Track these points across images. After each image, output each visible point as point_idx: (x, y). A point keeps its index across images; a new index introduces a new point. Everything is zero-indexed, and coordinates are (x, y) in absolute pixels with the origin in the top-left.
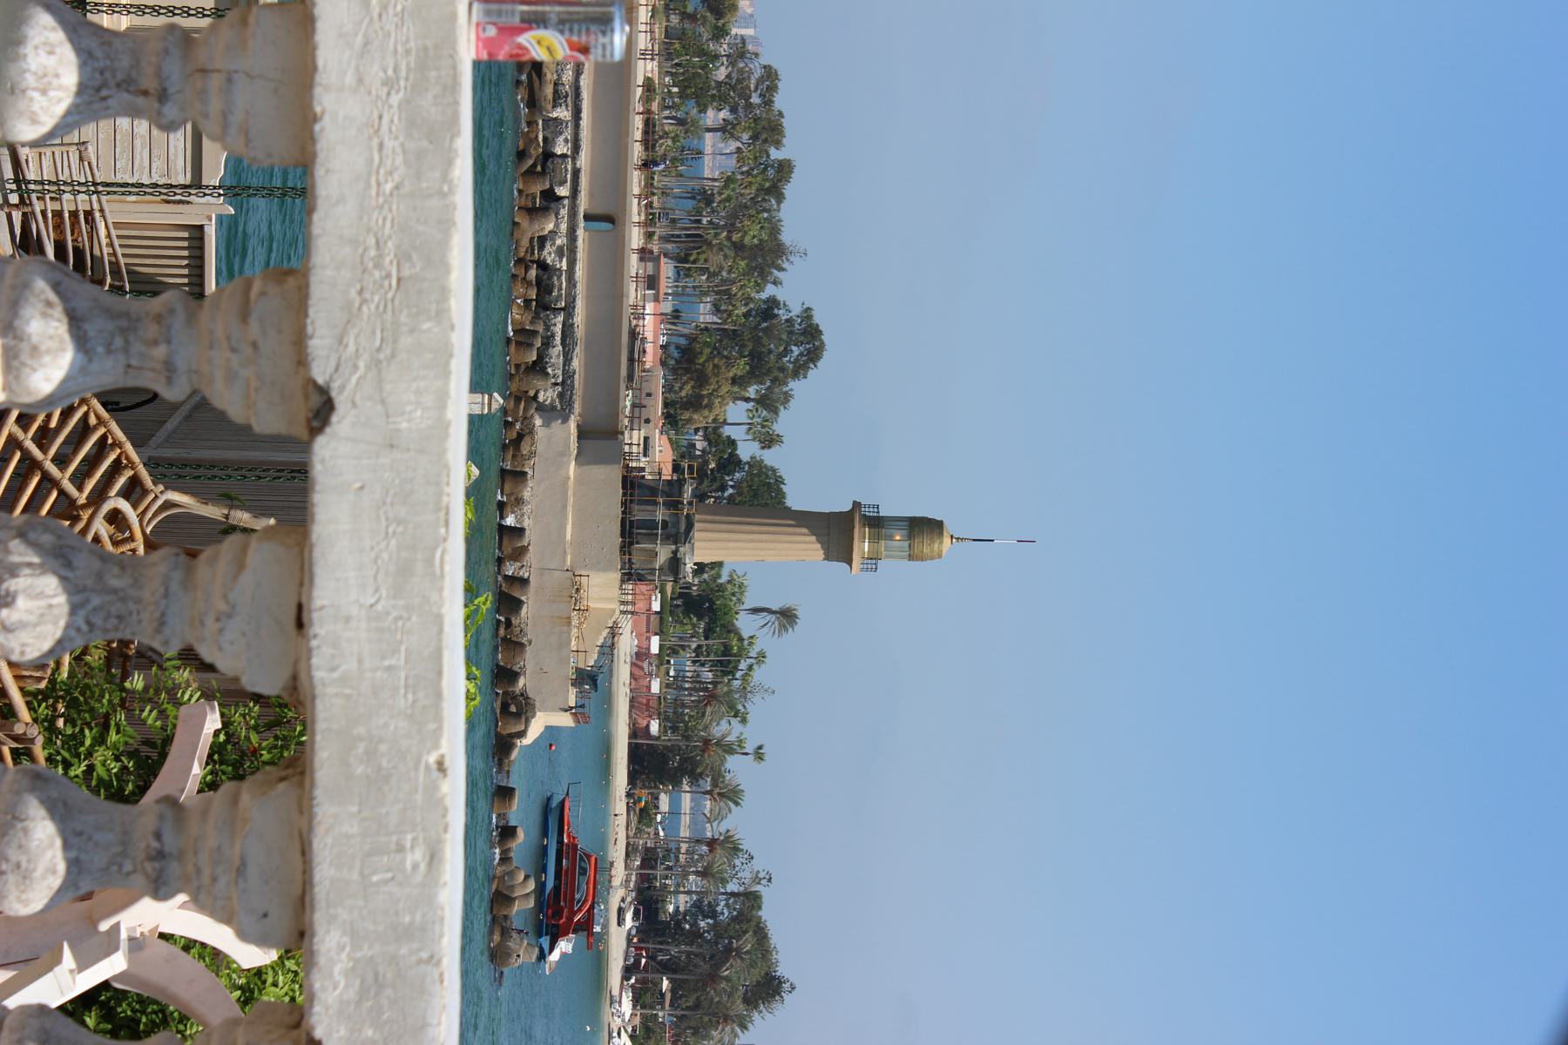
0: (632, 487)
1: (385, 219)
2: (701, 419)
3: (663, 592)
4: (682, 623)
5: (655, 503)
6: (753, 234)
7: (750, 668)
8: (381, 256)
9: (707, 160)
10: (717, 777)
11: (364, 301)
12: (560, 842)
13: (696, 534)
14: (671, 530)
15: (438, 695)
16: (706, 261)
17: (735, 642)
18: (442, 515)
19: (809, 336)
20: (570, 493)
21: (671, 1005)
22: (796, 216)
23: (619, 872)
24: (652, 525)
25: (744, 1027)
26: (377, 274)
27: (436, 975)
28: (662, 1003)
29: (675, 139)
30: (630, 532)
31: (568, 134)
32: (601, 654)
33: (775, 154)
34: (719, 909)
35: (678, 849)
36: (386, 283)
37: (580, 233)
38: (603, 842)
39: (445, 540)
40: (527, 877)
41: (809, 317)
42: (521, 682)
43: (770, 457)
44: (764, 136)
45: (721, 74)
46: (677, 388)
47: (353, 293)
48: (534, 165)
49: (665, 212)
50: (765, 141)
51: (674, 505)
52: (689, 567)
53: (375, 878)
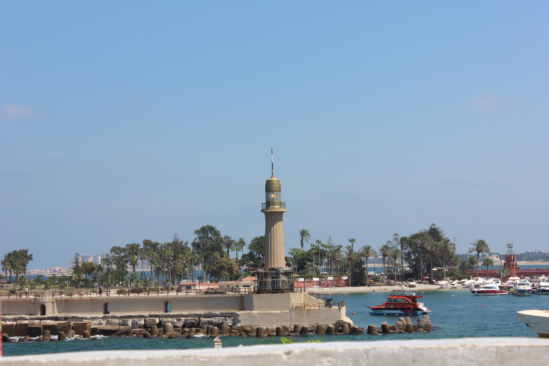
31: (137, 320)
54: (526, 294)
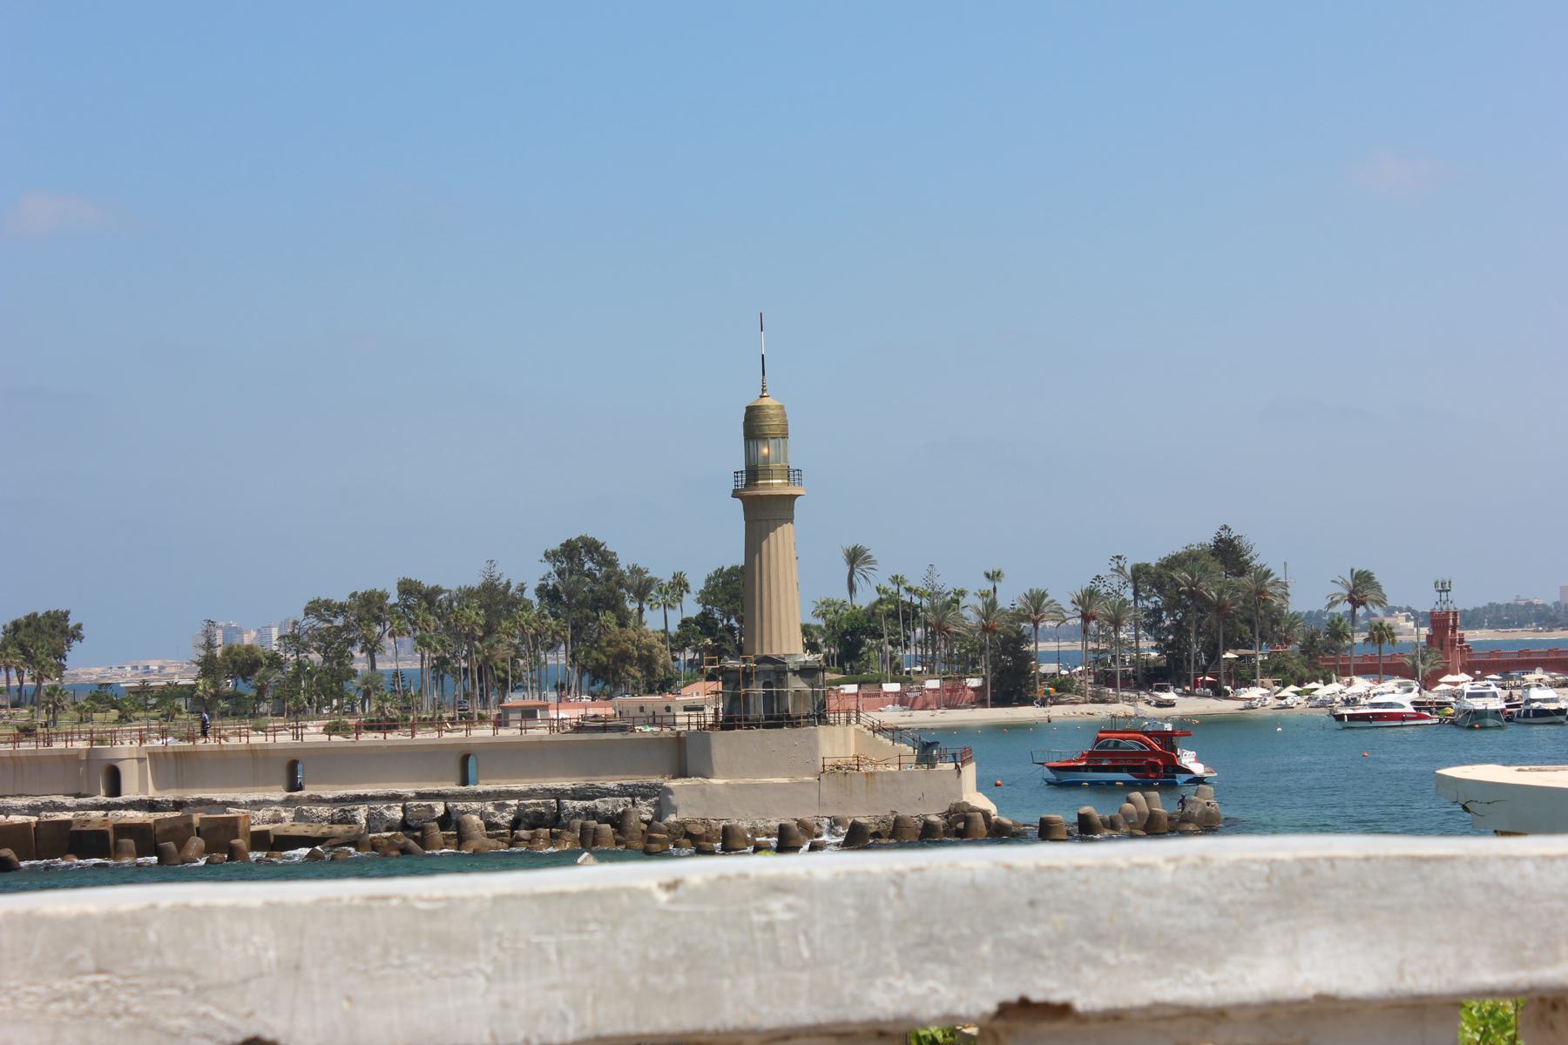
0: (731, 719)
1: (28, 993)
2: (663, 656)
3: (838, 683)
4: (868, 661)
5: (746, 695)
6: (475, 615)
7: (909, 590)
8: (73, 995)
9: (402, 666)
10: (1020, 616)
11: (127, 1011)
12: (1086, 769)
13: (775, 652)
14: (772, 678)
15: (588, 894)
16: (504, 660)
17: (884, 607)
18: (375, 904)
19: (573, 552)
20: (741, 781)
21: (1250, 648)
22: (453, 573)
23: (1121, 709)
24: (768, 698)
25: (1267, 574)
26: (94, 998)
27: (915, 876)
28: (1249, 657)
29: (384, 700)
30: (777, 719)
31: (381, 807)
32: (901, 740)
33: (394, 599)
34: (1151, 606)
35: (1094, 651)
36: (104, 987)
37: (480, 788)
38: (1089, 726)
39: (405, 899)
40: (1129, 801)
41: (555, 553)
42: (934, 819)
43: (697, 583)
44: (376, 611)
45: (316, 657)
46: (631, 681)
47: (118, 1024)
48: (415, 839)
49: (458, 705)
50: (381, 609)
51: (747, 676)
52: (808, 657)
53: (806, 953)
54: (1490, 722)
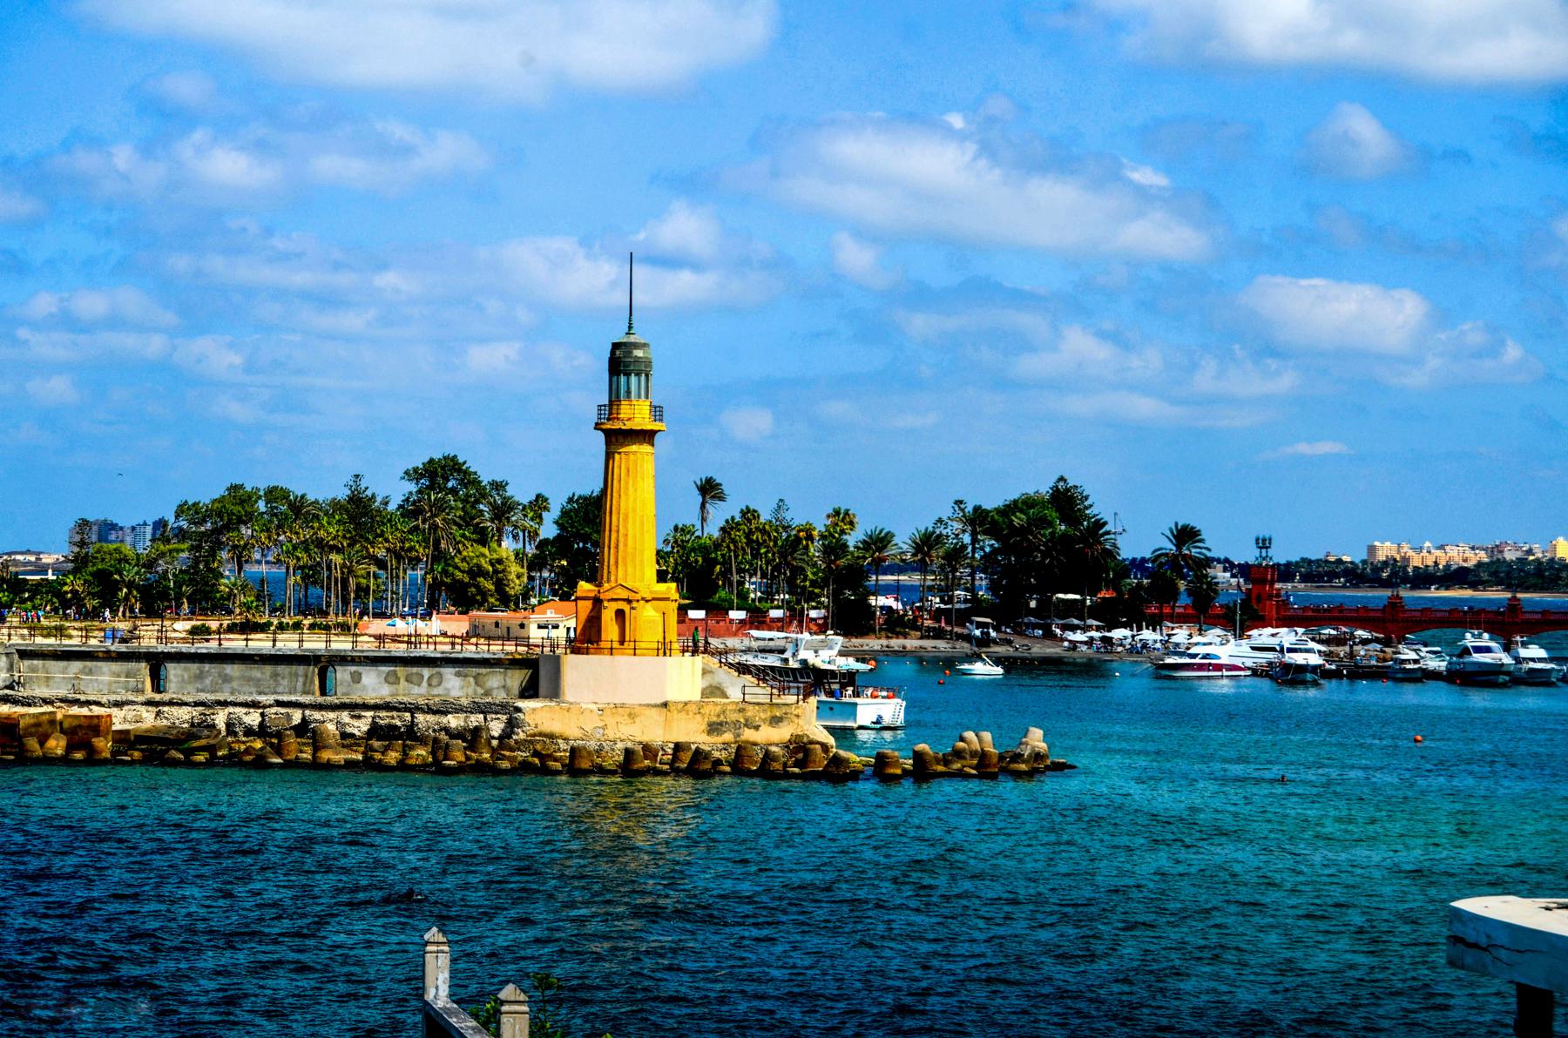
31: (240, 711)
54: (1309, 677)
